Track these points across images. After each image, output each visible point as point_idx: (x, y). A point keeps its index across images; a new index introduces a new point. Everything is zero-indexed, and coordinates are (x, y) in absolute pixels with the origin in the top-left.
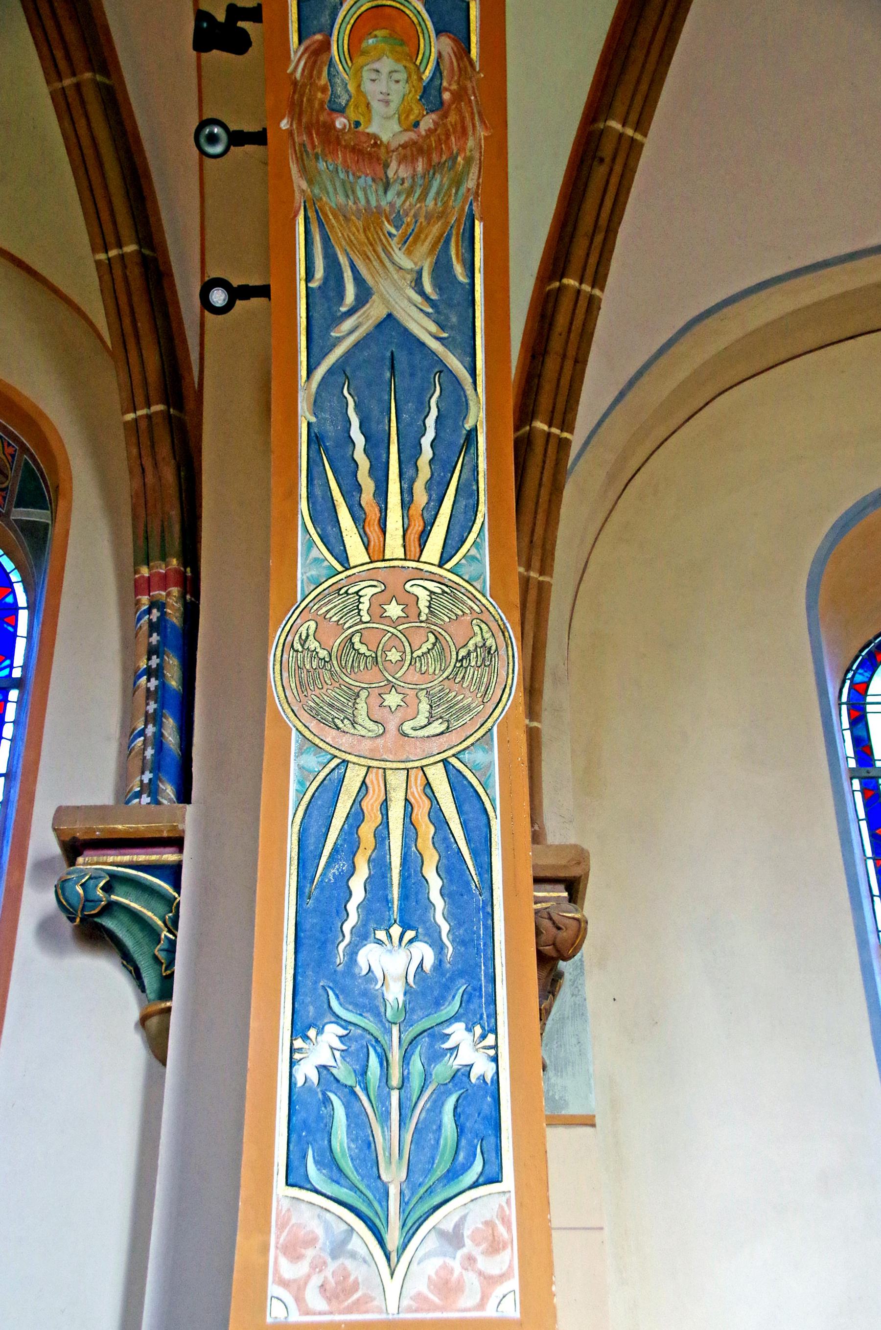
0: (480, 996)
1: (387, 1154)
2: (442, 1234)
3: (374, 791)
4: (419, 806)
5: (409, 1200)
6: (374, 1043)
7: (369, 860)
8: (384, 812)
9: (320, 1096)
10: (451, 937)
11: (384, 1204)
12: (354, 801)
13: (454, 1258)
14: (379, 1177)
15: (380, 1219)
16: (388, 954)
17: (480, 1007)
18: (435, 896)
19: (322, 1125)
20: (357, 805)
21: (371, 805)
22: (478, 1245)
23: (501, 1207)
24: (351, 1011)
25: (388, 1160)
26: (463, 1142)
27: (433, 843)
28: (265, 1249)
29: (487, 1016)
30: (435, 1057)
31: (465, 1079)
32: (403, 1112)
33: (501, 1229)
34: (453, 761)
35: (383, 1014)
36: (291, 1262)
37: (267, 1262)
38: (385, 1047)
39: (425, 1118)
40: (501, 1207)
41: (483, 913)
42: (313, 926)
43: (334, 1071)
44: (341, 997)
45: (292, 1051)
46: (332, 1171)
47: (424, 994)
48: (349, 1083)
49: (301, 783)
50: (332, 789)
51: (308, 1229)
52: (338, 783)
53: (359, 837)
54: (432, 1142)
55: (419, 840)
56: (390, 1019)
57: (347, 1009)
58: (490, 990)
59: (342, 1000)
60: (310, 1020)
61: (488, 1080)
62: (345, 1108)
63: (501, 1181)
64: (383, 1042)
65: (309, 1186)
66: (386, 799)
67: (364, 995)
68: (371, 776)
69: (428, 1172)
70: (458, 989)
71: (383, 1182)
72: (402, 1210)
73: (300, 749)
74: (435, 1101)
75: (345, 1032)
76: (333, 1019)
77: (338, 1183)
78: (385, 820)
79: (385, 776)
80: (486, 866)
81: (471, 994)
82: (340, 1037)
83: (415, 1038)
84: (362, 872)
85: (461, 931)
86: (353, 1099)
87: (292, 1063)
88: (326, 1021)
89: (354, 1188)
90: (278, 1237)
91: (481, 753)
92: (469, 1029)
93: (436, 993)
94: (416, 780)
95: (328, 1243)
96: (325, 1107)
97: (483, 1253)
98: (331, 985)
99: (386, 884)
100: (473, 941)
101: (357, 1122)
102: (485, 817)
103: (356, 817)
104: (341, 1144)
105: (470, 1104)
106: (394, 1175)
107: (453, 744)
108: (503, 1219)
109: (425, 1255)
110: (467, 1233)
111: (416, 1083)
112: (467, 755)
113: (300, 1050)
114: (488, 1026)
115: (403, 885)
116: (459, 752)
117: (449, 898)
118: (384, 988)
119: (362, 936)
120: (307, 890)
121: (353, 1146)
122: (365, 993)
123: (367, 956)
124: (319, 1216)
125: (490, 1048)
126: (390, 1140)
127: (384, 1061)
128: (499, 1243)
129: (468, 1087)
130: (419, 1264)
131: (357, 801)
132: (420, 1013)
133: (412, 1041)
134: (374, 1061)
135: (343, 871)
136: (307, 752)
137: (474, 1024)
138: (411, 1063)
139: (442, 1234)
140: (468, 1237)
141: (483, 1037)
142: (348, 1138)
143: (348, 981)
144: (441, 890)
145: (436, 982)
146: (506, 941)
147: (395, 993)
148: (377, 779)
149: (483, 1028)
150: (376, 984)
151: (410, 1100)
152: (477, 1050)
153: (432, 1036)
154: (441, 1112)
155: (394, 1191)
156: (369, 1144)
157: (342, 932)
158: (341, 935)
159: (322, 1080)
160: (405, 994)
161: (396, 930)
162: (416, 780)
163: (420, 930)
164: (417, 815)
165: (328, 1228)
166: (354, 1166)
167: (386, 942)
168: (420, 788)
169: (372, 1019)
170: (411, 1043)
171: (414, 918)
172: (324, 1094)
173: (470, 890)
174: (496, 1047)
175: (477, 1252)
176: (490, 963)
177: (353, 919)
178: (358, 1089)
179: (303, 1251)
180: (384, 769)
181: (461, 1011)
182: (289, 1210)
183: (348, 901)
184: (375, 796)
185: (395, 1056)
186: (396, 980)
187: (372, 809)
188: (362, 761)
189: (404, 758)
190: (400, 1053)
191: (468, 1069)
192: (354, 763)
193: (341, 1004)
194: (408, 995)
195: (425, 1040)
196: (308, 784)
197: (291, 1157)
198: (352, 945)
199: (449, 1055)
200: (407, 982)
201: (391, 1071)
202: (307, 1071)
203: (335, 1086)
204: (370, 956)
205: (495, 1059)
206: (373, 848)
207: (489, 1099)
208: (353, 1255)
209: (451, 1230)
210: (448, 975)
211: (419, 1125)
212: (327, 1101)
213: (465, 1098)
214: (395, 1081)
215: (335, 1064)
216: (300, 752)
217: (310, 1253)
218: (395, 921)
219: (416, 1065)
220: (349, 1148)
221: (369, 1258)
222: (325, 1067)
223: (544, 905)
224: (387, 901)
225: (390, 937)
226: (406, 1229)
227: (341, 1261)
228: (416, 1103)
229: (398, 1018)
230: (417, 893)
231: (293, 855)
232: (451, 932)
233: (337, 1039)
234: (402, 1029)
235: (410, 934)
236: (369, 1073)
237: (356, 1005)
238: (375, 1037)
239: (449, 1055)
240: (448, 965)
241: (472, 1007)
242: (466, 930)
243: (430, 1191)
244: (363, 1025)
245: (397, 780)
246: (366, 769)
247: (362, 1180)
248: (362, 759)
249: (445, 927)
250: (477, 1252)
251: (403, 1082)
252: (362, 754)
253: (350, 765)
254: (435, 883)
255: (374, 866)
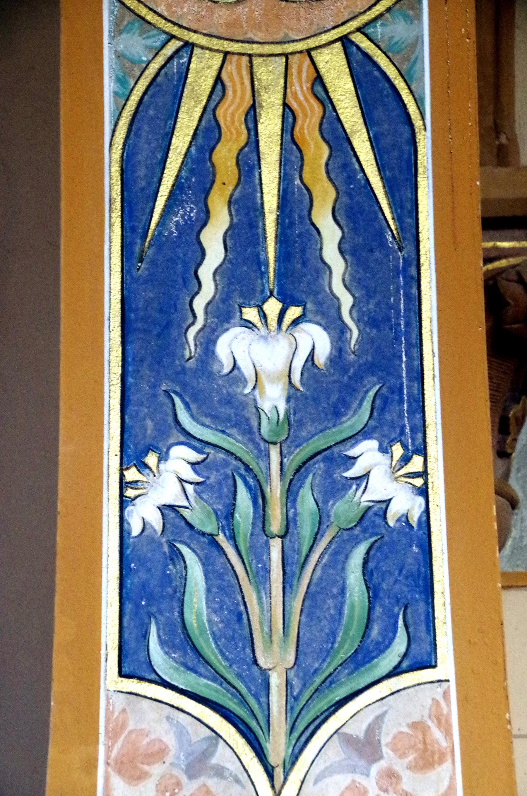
0: (401, 401)
1: (266, 629)
2: (349, 741)
3: (235, 92)
4: (305, 115)
5: (301, 692)
6: (242, 471)
7: (230, 203)
8: (251, 126)
9: (166, 549)
10: (355, 314)
11: (263, 699)
12: (205, 108)
13: (368, 775)
14: (255, 662)
15: (258, 723)
16: (262, 342)
17: (401, 416)
18: (331, 253)
19: (170, 590)
20: (209, 115)
21: (231, 114)
22: (402, 756)
23: (435, 702)
24: (208, 426)
25: (268, 639)
26: (378, 610)
27: (328, 172)
28: (91, 766)
29: (411, 430)
30: (334, 489)
31: (379, 521)
32: (288, 569)
33: (437, 734)
34: (358, 39)
35: (255, 430)
36: (129, 784)
37: (95, 786)
38: (262, 480)
39: (321, 578)
40: (435, 702)
41: (404, 278)
42: (148, 302)
43: (186, 513)
44: (193, 406)
45: (123, 485)
46: (185, 654)
47: (316, 400)
48: (208, 530)
49: (121, 81)
50: (167, 90)
51: (153, 737)
52: (179, 81)
53: (213, 166)
54: (332, 612)
55: (306, 169)
56: (266, 437)
57: (203, 425)
58: (416, 392)
59: (194, 411)
60: (148, 441)
61: (414, 523)
62: (203, 564)
63: (435, 666)
64: (256, 470)
65: (153, 676)
66: (253, 107)
67: (225, 400)
68: (229, 67)
69: (326, 654)
70: (367, 392)
71: (261, 668)
72: (289, 709)
73: (117, 25)
74: (336, 553)
75: (200, 457)
76: (182, 439)
77: (196, 672)
78: (253, 137)
79: (251, 67)
80: (408, 206)
81: (387, 398)
82: (193, 464)
83: (304, 463)
84: (220, 221)
85: (371, 306)
86: (215, 553)
87: (124, 502)
88: (171, 441)
89: (218, 677)
90: (109, 749)
91: (403, 22)
92: (384, 450)
93: (334, 398)
94: (300, 72)
95: (182, 757)
96: (174, 564)
97: (409, 768)
98: (178, 389)
99: (255, 236)
100: (389, 319)
101: (222, 584)
102: (407, 128)
103: (209, 133)
104: (199, 616)
105: (386, 557)
106: (276, 660)
107: (358, 10)
108: (438, 719)
109: (324, 771)
110: (385, 739)
111: (306, 529)
112: (379, 29)
113: (134, 484)
114: (413, 444)
115: (282, 238)
116: (367, 24)
117: (353, 255)
118: (257, 392)
119: (223, 315)
120: (137, 249)
121: (216, 619)
122: (228, 400)
123: (230, 346)
124: (168, 718)
125: (416, 475)
126: (272, 611)
127: (259, 497)
128: (433, 753)
129: (384, 531)
130: (315, 783)
131: (210, 110)
132: (311, 428)
133: (300, 467)
134: (244, 498)
135: (190, 218)
136: (128, 29)
137: (392, 442)
138: (299, 499)
139: (349, 741)
140: (387, 745)
141: (406, 460)
142: (208, 607)
143: (202, 383)
144: (340, 244)
145: (334, 382)
146: (439, 317)
147: (273, 399)
148: (240, 73)
149: (405, 446)
150: (245, 387)
151: (299, 552)
152: (396, 479)
153: (330, 461)
154: (343, 569)
155: (276, 681)
156: (239, 616)
157: (192, 310)
158: (190, 315)
159: (168, 526)
160: (288, 400)
161: (273, 307)
162: (300, 72)
163: (309, 306)
164: (302, 128)
165: (181, 733)
166: (218, 646)
167: (259, 324)
168: (306, 86)
169: (239, 438)
170: (297, 471)
171: (299, 284)
172: (171, 546)
173: (383, 243)
174: (424, 474)
175: (400, 766)
176: (415, 352)
177: (208, 290)
178: (221, 538)
179: (146, 768)
180: (250, 56)
181: (372, 423)
182: (124, 711)
183: (200, 264)
184: (237, 101)
185: (275, 490)
186: (273, 380)
187: (233, 122)
188: (215, 44)
189: (279, 37)
190: (282, 486)
191: (384, 506)
192: (202, 48)
193: (192, 416)
194: (292, 402)
195: (319, 466)
196: (132, 83)
197: (126, 636)
198: (207, 330)
199: (354, 487)
200: (290, 382)
201: (269, 511)
202: (145, 513)
203: (187, 533)
204: (235, 346)
205: (424, 492)
206: (235, 182)
207: (415, 549)
208: (219, 772)
209: (362, 735)
210: (352, 371)
211: (312, 587)
212: (176, 556)
213: (379, 549)
214: (276, 525)
215: (186, 504)
216: (118, 30)
217: (157, 770)
218: (272, 294)
219: (307, 502)
220: (210, 621)
221: (243, 777)
222: (171, 507)
223: (512, 261)
224: (259, 263)
225: (264, 316)
226: (296, 734)
227: (202, 779)
228: (307, 556)
229: (278, 435)
230: (303, 252)
231: (114, 194)
232: (356, 308)
233: (189, 466)
234: (285, 451)
235: (294, 312)
236: (237, 515)
237: (215, 418)
238: (244, 464)
239: (354, 487)
240: (352, 356)
241: (388, 417)
242: (378, 304)
243: (330, 681)
244: (226, 446)
245: (269, 73)
246: (221, 55)
247: (231, 666)
248: (215, 41)
249: (346, 301)
250: (400, 766)
251: (287, 528)
252: (214, 31)
253: (197, 51)
254: (331, 234)
255: (237, 210)
